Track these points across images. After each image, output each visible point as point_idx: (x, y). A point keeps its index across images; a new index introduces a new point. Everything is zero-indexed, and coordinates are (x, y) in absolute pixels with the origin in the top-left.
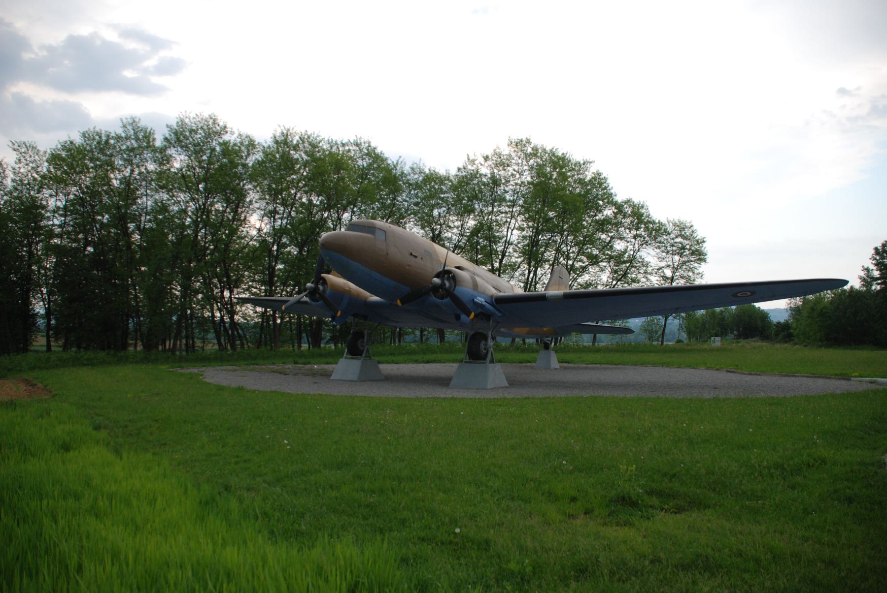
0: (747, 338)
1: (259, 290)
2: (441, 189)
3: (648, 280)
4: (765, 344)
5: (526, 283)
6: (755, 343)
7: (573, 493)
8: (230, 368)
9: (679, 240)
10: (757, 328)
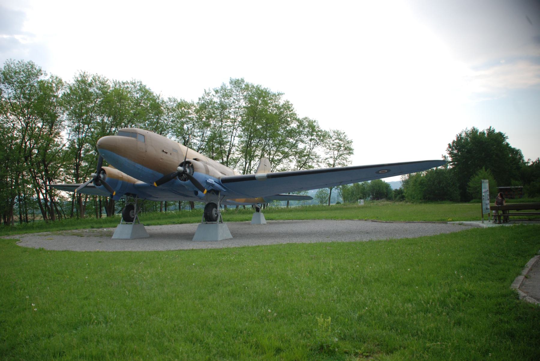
0: (378, 199)
1: (71, 180)
2: (189, 112)
3: (319, 166)
4: (388, 202)
5: (244, 171)
6: (383, 203)
7: (278, 344)
8: (45, 233)
9: (337, 141)
10: (382, 193)
